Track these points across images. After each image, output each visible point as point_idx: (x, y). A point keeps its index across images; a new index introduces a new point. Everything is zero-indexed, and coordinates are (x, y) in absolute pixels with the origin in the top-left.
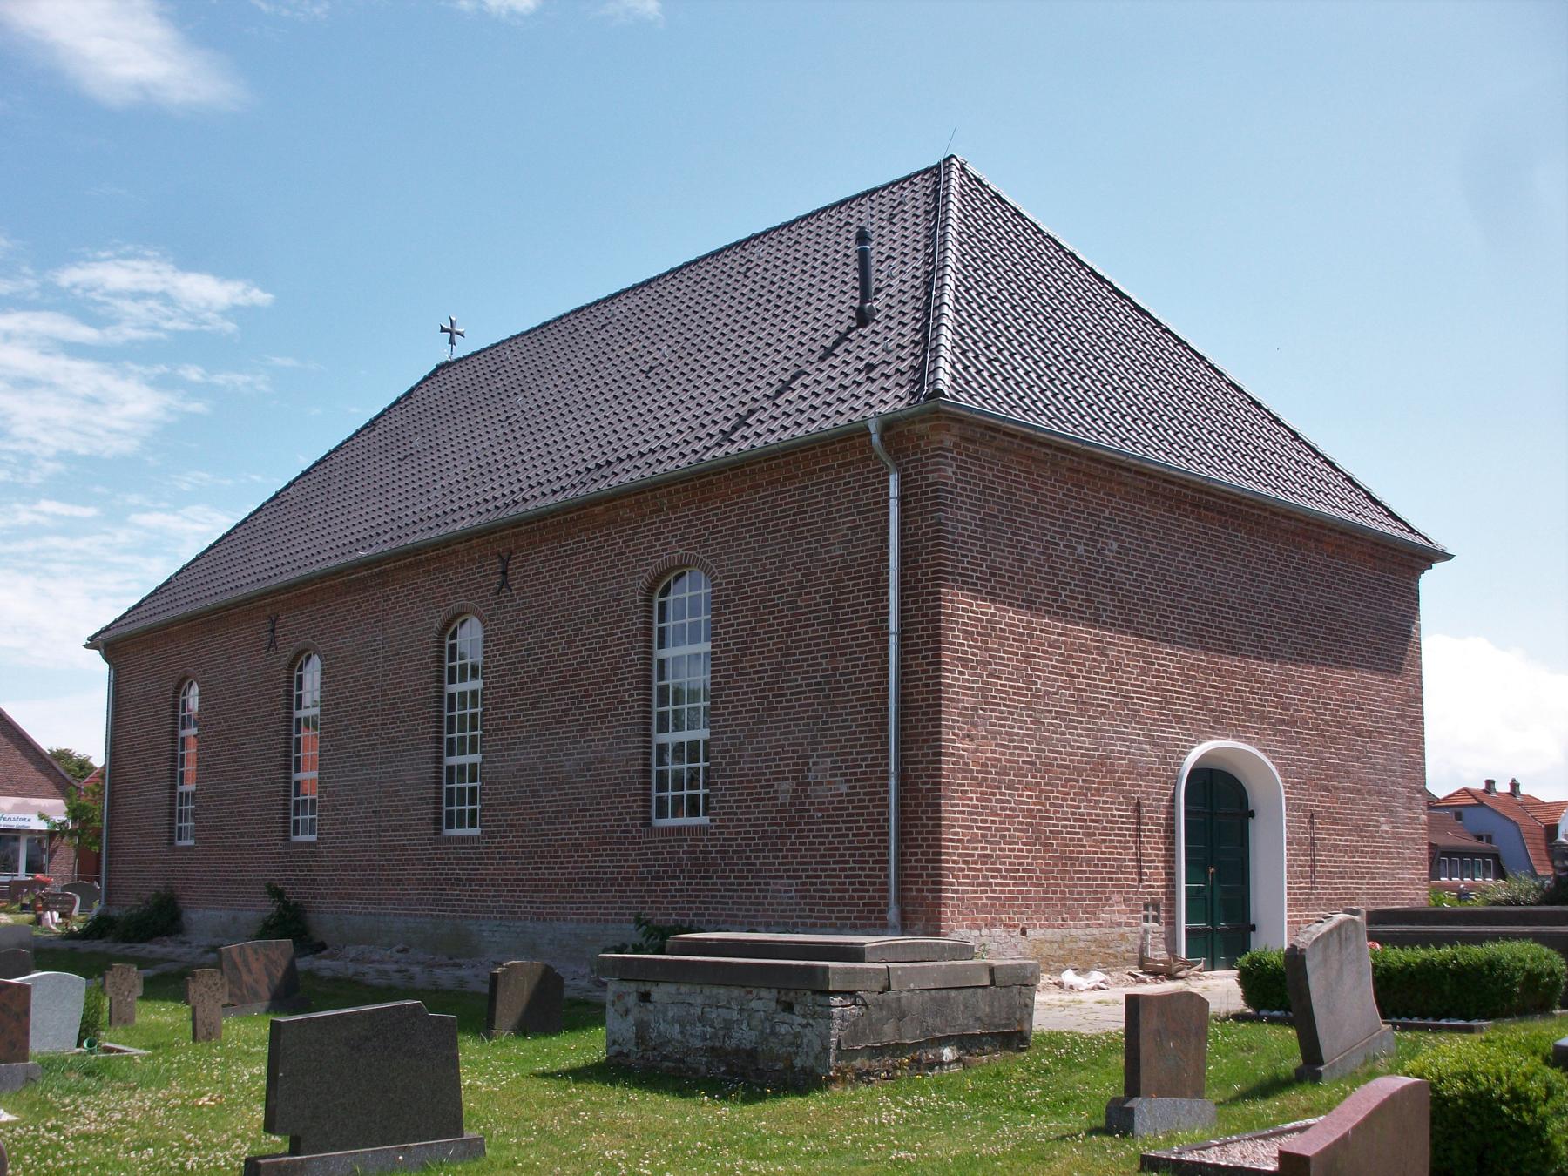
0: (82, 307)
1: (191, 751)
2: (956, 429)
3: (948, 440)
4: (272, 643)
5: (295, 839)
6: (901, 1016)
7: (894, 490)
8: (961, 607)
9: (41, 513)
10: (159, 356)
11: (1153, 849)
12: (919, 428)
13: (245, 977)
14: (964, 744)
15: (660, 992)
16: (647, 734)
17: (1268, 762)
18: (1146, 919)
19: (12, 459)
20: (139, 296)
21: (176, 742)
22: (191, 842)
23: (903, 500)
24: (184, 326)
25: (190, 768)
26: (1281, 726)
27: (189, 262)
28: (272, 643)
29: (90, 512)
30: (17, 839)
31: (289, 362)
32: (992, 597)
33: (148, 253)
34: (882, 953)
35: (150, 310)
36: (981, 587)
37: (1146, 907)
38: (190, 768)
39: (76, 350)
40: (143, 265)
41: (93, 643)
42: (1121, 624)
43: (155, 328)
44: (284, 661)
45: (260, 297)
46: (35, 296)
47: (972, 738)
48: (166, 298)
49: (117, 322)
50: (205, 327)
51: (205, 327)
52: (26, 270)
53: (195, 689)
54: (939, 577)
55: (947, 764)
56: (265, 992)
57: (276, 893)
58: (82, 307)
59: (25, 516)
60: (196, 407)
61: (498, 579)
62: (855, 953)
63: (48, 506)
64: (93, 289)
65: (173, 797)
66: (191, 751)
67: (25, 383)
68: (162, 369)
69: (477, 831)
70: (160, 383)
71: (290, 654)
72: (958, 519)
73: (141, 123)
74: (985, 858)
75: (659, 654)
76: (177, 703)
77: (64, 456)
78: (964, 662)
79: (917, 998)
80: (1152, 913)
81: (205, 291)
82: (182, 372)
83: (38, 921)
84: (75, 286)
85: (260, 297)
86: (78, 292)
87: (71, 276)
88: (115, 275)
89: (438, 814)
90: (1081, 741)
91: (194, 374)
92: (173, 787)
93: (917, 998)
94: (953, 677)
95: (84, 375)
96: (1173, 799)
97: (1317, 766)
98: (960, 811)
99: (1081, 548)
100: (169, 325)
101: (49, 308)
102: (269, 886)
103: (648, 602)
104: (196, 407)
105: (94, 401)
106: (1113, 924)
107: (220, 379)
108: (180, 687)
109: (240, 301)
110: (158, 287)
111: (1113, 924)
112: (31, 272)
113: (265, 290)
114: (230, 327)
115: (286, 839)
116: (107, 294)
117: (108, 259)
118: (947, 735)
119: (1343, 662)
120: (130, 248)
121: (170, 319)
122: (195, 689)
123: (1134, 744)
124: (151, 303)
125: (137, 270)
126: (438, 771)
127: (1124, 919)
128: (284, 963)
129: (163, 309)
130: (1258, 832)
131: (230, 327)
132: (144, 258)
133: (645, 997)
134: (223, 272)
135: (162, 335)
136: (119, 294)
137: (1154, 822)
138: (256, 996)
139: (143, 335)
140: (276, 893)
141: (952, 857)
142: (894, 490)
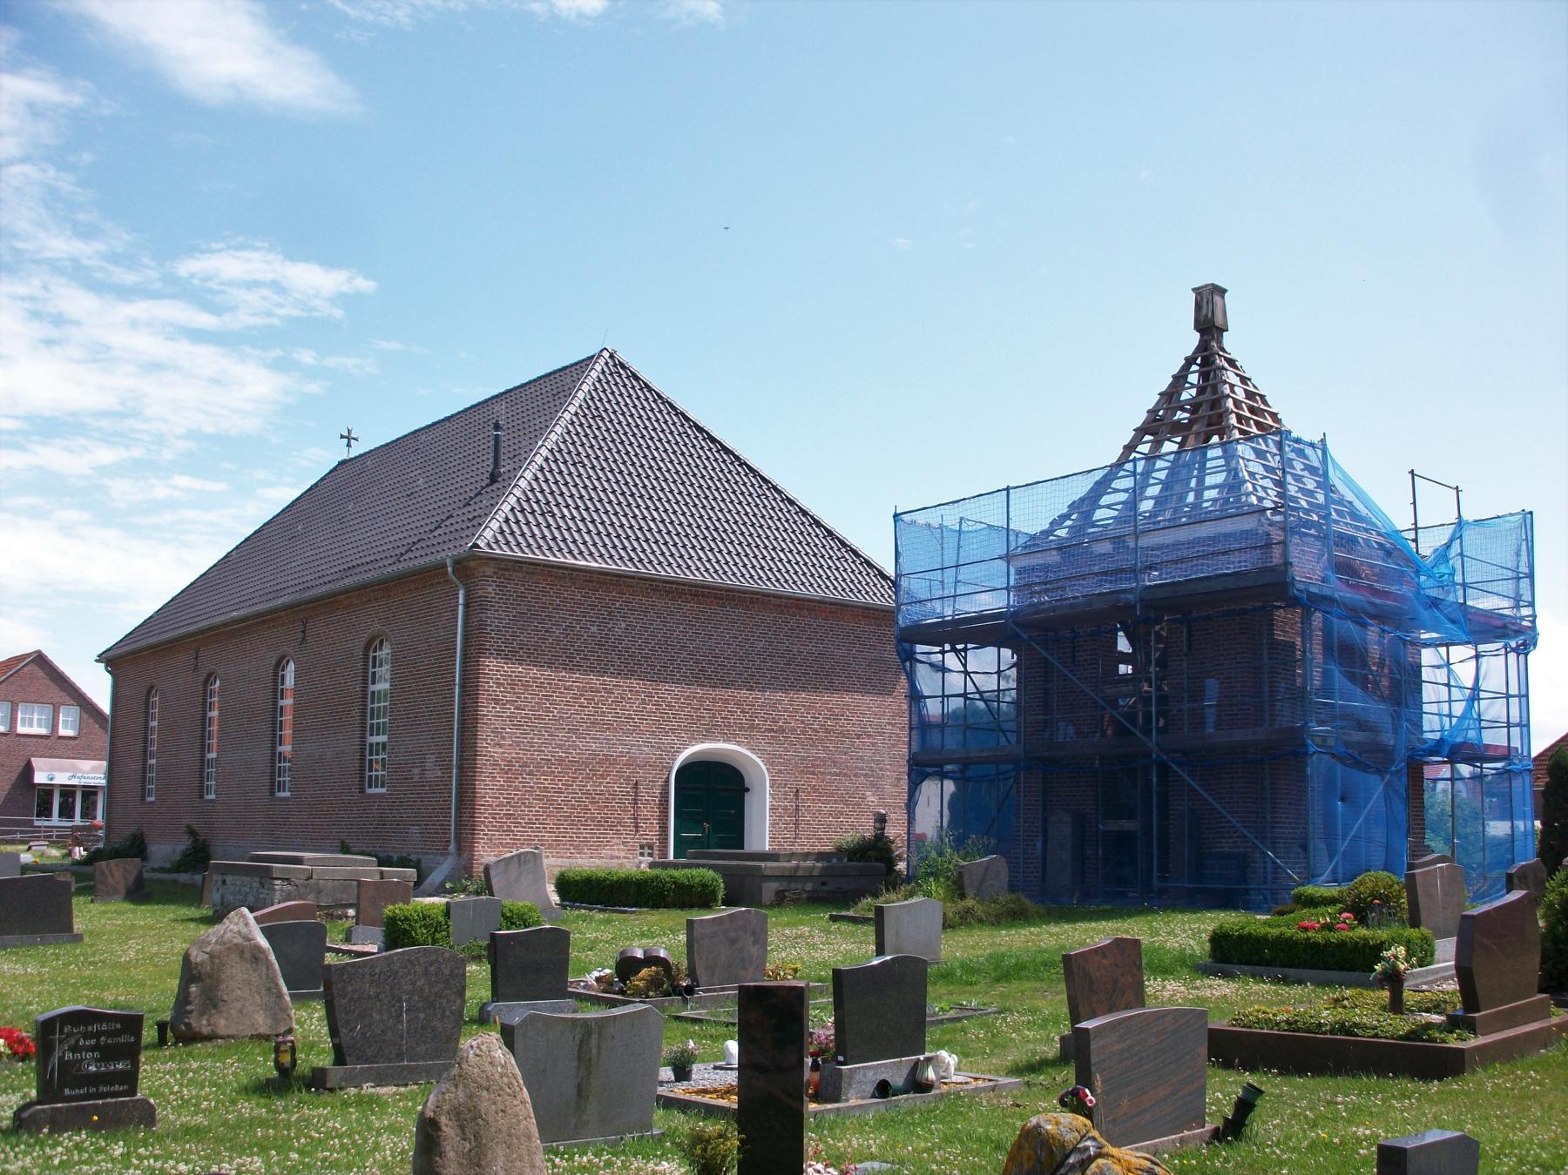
0: (201, 295)
1: (288, 718)
2: (492, 564)
3: (489, 571)
4: (196, 667)
5: (369, 791)
6: (320, 892)
7: (461, 601)
8: (494, 669)
9: (176, 488)
10: (274, 341)
11: (649, 812)
12: (473, 564)
13: (110, 880)
14: (492, 750)
15: (229, 879)
16: (363, 737)
17: (754, 757)
18: (642, 854)
19: (147, 438)
20: (252, 285)
21: (276, 711)
22: (288, 794)
23: (466, 606)
24: (296, 313)
25: (287, 732)
26: (745, 731)
27: (297, 247)
28: (196, 667)
29: (219, 486)
30: (95, 794)
31: (393, 346)
32: (520, 661)
33: (259, 244)
34: (313, 861)
35: (264, 298)
36: (511, 655)
37: (642, 847)
38: (287, 732)
39: (197, 336)
40: (255, 255)
41: (101, 658)
42: (626, 671)
43: (270, 315)
44: (202, 679)
45: (365, 285)
46: (157, 285)
47: (501, 746)
48: (277, 286)
49: (231, 309)
50: (315, 314)
51: (315, 314)
52: (146, 261)
53: (292, 666)
54: (482, 651)
55: (480, 761)
56: (123, 890)
57: (192, 832)
58: (201, 295)
59: (161, 491)
60: (313, 388)
61: (300, 635)
62: (298, 861)
63: (182, 481)
64: (208, 279)
65: (275, 757)
66: (288, 718)
67: (155, 367)
68: (277, 352)
69: (383, 790)
70: (279, 366)
71: (365, 637)
72: (495, 618)
73: (239, 121)
74: (508, 816)
75: (281, 703)
76: (278, 678)
77: (194, 435)
78: (497, 701)
79: (330, 884)
80: (647, 851)
81: (315, 280)
82: (295, 356)
83: (70, 854)
84: (192, 276)
85: (365, 285)
86: (196, 282)
87: (189, 267)
88: (228, 265)
89: (273, 783)
90: (591, 745)
91: (307, 357)
92: (274, 747)
93: (330, 884)
94: (487, 710)
95: (207, 358)
96: (667, 781)
97: (803, 758)
98: (489, 788)
99: (594, 629)
100: (281, 312)
101: (171, 297)
102: (188, 826)
103: (366, 655)
104: (313, 388)
105: (216, 382)
106: (612, 857)
107: (332, 362)
108: (280, 664)
109: (346, 288)
110: (269, 277)
111: (612, 857)
112: (151, 264)
113: (368, 277)
114: (338, 313)
115: (201, 797)
116: (223, 283)
117: (219, 251)
118: (481, 744)
119: (832, 688)
120: (241, 239)
121: (282, 306)
122: (292, 666)
123: (641, 747)
124: (264, 292)
125: (248, 261)
126: (273, 754)
127: (622, 854)
128: (135, 872)
129: (275, 297)
130: (750, 801)
131: (338, 313)
132: (254, 248)
133: (224, 882)
134: (329, 261)
135: (276, 322)
136: (231, 284)
137: (650, 795)
138: (116, 891)
139: (259, 321)
140: (192, 832)
141: (483, 815)
142: (461, 601)
